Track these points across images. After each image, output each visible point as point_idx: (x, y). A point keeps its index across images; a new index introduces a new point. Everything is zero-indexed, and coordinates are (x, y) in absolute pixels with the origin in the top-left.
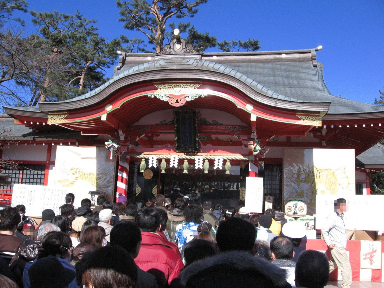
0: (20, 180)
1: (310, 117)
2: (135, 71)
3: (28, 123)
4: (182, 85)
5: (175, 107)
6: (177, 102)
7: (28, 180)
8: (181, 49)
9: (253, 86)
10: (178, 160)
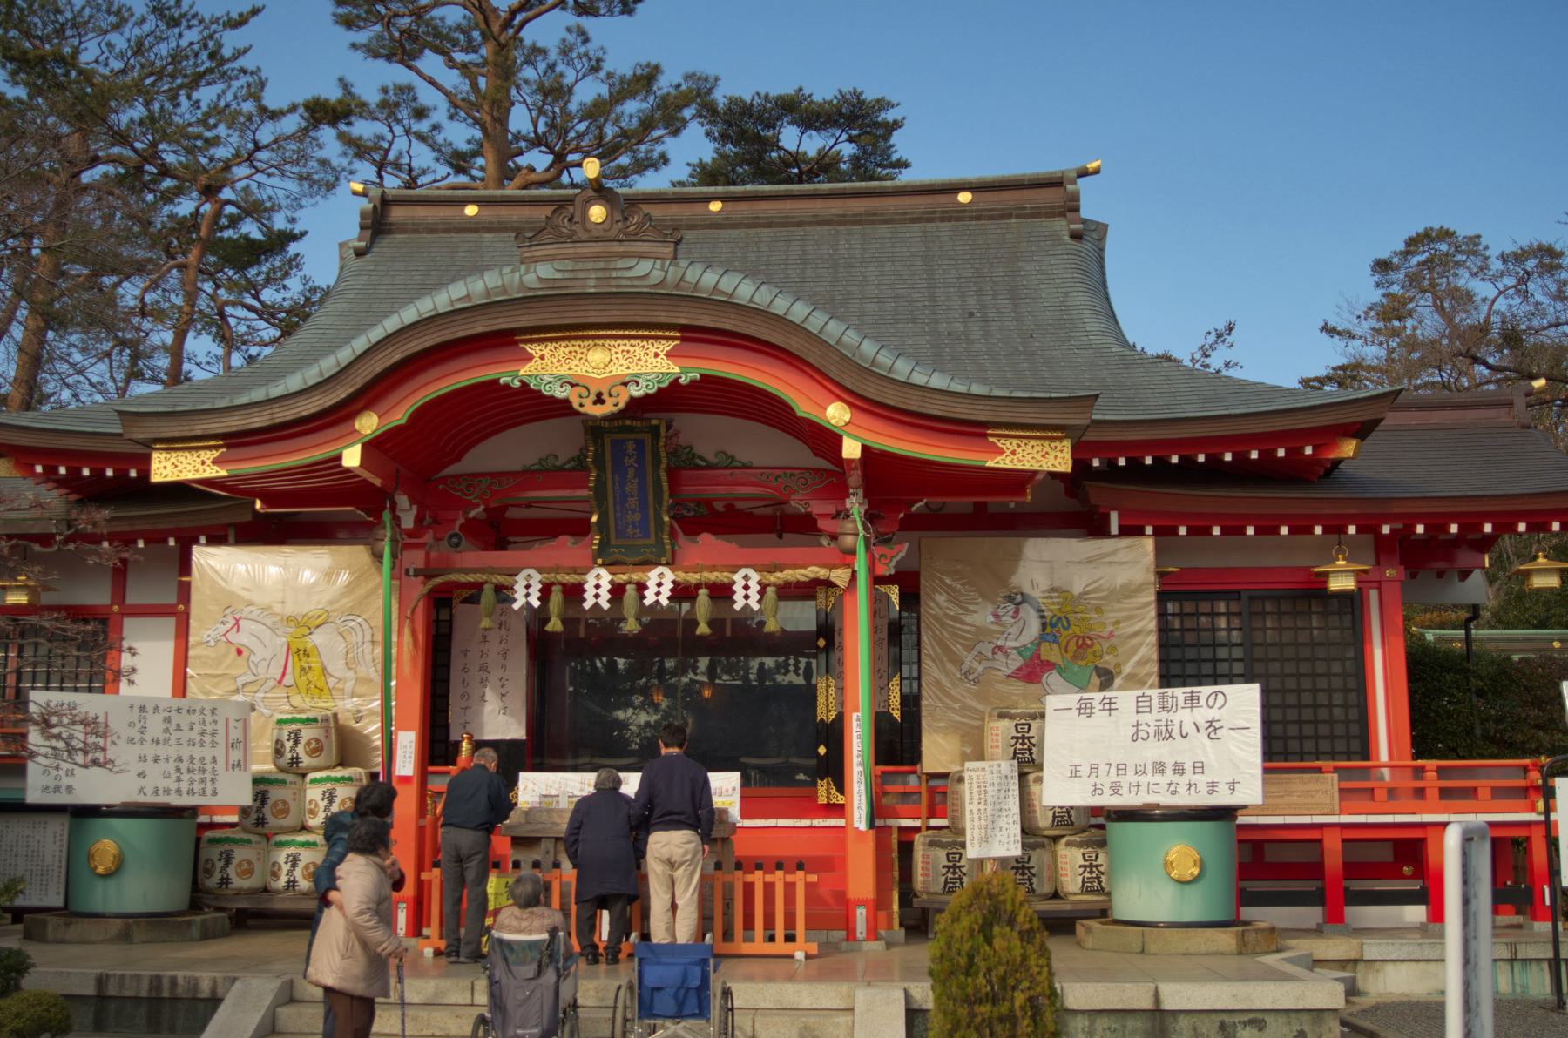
1: (1033, 442)
2: (459, 300)
3: (50, 471)
4: (612, 343)
5: (594, 418)
6: (599, 400)
8: (609, 221)
9: (847, 347)
10: (610, 591)
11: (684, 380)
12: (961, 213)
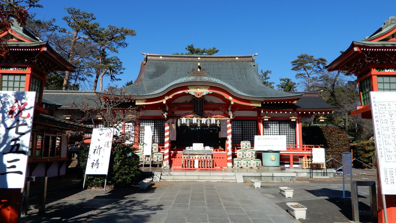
0: (278, 133)
7: (267, 133)
11: (210, 93)
12: (235, 61)
